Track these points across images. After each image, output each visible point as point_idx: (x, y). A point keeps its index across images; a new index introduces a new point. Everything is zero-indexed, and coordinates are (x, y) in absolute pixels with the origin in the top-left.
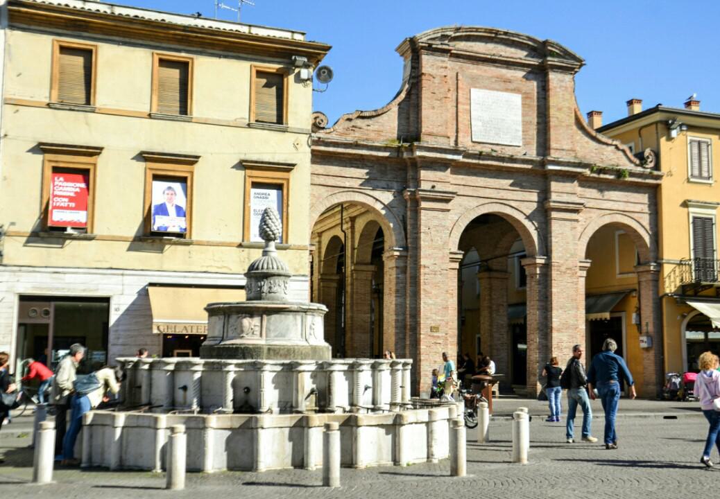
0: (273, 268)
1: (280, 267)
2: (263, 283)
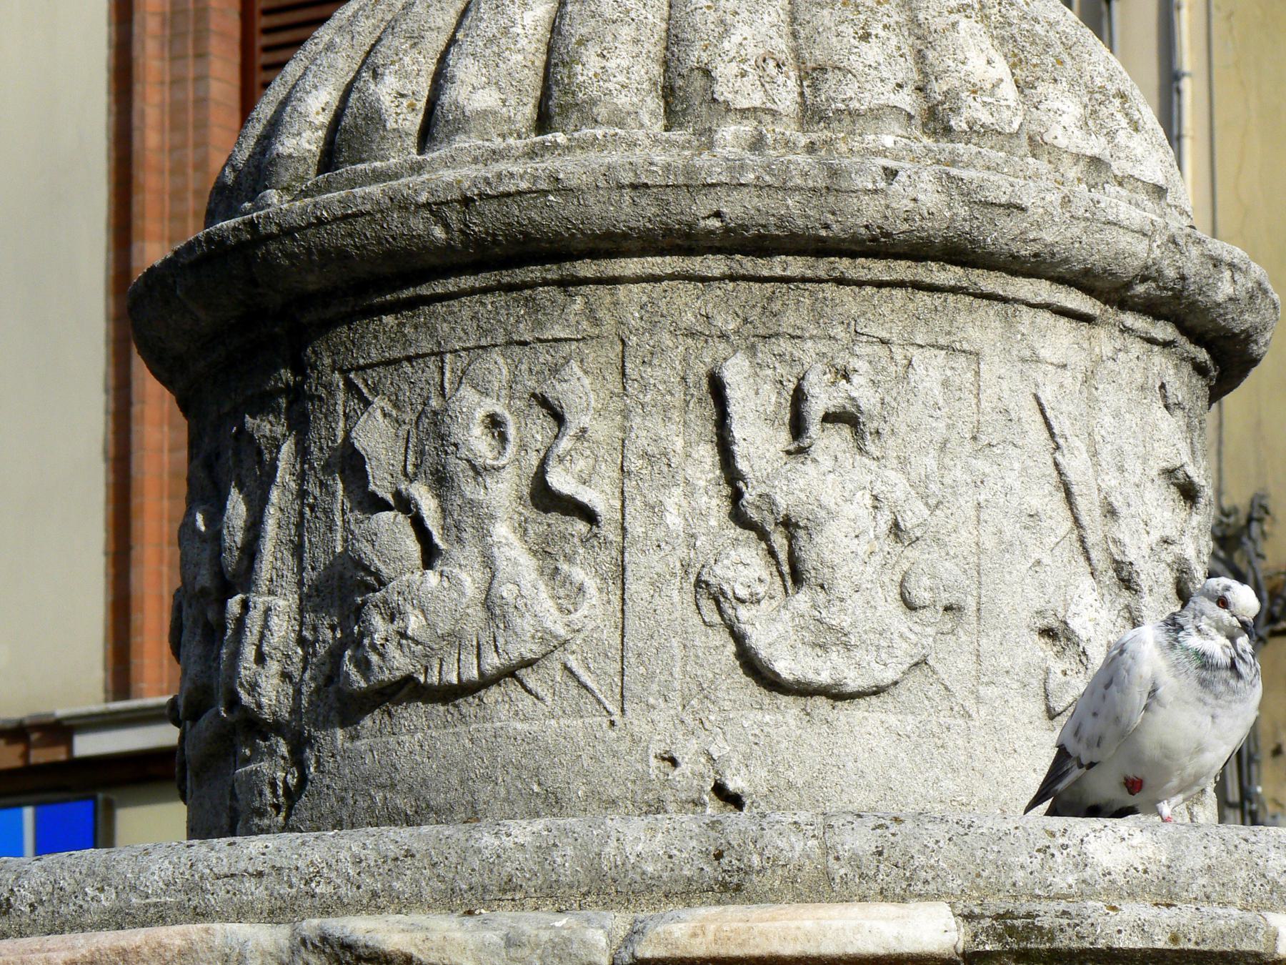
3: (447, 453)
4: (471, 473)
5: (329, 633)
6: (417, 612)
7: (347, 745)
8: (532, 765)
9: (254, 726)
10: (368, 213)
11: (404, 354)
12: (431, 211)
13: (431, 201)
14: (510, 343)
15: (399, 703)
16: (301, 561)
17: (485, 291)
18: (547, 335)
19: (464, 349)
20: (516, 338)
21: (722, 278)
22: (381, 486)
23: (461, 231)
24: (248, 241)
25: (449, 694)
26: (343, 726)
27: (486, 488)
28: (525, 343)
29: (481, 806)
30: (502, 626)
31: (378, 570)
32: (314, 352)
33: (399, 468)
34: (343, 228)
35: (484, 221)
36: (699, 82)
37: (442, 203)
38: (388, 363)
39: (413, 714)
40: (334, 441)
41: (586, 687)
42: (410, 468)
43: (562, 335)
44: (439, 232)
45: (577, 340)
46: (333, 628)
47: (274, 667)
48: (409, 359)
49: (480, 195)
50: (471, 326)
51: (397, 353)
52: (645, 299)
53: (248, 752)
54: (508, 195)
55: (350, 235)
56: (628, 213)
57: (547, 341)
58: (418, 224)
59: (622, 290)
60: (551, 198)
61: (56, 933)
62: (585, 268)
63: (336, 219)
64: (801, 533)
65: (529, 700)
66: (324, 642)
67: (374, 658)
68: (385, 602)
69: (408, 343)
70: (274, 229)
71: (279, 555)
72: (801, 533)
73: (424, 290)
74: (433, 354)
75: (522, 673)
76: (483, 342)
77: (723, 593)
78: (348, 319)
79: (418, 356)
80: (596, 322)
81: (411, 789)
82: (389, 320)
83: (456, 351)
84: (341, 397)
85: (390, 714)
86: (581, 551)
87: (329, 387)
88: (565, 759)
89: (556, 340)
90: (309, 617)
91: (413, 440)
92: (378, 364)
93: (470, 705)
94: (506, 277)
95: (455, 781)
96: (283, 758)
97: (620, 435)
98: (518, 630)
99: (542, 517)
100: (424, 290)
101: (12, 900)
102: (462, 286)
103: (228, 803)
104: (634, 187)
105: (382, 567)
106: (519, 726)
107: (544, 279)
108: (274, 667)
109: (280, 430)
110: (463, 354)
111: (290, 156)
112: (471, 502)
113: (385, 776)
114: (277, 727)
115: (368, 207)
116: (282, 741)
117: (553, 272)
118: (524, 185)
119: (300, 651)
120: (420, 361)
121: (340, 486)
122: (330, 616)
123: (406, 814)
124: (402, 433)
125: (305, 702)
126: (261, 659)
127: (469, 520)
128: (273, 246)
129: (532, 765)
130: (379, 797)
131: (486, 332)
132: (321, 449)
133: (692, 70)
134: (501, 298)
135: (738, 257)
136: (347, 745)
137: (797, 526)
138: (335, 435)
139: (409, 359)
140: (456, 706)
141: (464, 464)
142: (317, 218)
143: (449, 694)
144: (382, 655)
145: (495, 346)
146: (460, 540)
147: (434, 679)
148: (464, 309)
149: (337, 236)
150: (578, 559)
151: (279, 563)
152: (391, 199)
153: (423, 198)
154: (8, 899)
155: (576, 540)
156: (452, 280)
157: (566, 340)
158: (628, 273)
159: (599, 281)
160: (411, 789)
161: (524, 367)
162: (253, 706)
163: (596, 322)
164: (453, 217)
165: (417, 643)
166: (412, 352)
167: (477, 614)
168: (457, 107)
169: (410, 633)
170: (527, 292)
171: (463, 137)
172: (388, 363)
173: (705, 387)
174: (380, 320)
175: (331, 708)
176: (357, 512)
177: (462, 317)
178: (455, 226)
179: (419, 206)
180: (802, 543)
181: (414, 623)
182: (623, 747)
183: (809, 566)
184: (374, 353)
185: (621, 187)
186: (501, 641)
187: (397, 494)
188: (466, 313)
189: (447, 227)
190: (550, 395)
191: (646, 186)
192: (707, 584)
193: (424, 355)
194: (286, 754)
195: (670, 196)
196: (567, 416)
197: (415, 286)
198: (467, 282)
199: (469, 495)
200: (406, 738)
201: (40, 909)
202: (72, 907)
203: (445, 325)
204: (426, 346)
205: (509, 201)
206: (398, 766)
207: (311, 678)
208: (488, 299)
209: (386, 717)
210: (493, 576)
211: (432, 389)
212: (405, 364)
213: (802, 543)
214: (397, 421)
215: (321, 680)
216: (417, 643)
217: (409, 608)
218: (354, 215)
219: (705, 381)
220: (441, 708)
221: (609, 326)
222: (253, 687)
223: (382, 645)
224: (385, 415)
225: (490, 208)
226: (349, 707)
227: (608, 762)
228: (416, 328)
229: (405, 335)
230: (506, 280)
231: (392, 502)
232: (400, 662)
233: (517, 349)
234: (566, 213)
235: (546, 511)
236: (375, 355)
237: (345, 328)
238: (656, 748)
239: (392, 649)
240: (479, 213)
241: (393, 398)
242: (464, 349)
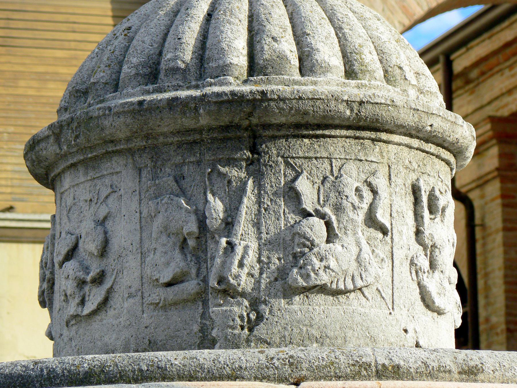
0: (307, 64)
1: (370, 57)
2: (217, 207)
3: (342, 199)
4: (352, 208)
5: (277, 261)
6: (334, 259)
7: (286, 306)
8: (366, 325)
9: (228, 292)
10: (323, 99)
11: (315, 156)
12: (347, 103)
13: (349, 100)
14: (355, 159)
15: (313, 293)
16: (259, 229)
17: (347, 137)
18: (369, 159)
19: (340, 158)
20: (359, 158)
21: (417, 149)
22: (309, 205)
23: (356, 114)
24: (259, 99)
25: (336, 293)
26: (284, 298)
27: (358, 215)
28: (361, 160)
29: (348, 339)
30: (363, 270)
31: (313, 240)
32: (266, 146)
33: (316, 200)
34: (311, 103)
35: (367, 111)
36: (398, 71)
37: (353, 101)
38: (306, 158)
39: (320, 299)
40: (280, 184)
41: (383, 298)
42: (322, 202)
43: (374, 160)
44: (348, 112)
45: (377, 163)
46: (279, 259)
47: (246, 270)
48: (316, 158)
49: (367, 101)
50: (342, 150)
51: (311, 154)
52: (396, 152)
53: (222, 302)
54: (377, 103)
55: (313, 106)
56: (408, 118)
57: (369, 161)
58: (342, 107)
59: (390, 146)
60: (390, 107)
61: (505, 383)
62: (384, 136)
63: (308, 99)
64: (437, 250)
65: (365, 299)
66: (274, 263)
67: (312, 274)
68: (319, 253)
69: (316, 151)
70: (276, 97)
71: (246, 225)
72: (437, 250)
73: (327, 132)
74: (327, 158)
75: (364, 289)
76: (347, 157)
77: (420, 269)
78: (287, 137)
79: (321, 158)
80: (382, 156)
81: (319, 328)
82: (306, 141)
83: (337, 158)
84: (282, 167)
85: (307, 297)
86: (380, 245)
87: (276, 163)
88: (377, 325)
89: (372, 161)
90: (265, 253)
91: (322, 191)
92: (301, 158)
93: (343, 298)
94: (358, 133)
95: (338, 328)
96: (246, 307)
97: (390, 203)
98: (371, 273)
99: (368, 229)
100: (327, 132)
101: (484, 367)
102: (342, 134)
103: (199, 321)
104: (414, 109)
105: (315, 238)
106: (360, 308)
107: (370, 137)
108: (246, 270)
109: (243, 175)
110: (339, 160)
111: (237, 65)
112: (352, 219)
113: (307, 321)
114: (243, 295)
115: (324, 97)
116: (245, 300)
117: (373, 135)
118: (383, 101)
119: (258, 265)
120: (321, 159)
121: (283, 203)
122: (278, 254)
123: (317, 338)
124: (316, 186)
125: (263, 286)
126: (241, 265)
127: (351, 226)
128: (272, 104)
129: (366, 325)
130: (305, 329)
131: (348, 154)
132: (272, 186)
133: (394, 65)
134: (353, 141)
135: (422, 141)
136: (286, 306)
137: (436, 247)
138: (280, 182)
139: (316, 158)
140: (337, 298)
141: (350, 204)
142: (299, 97)
143: (336, 293)
144: (316, 274)
145: (350, 159)
146: (346, 233)
147: (334, 286)
148: (341, 142)
149: (308, 106)
150: (379, 247)
151: (246, 229)
152: (332, 96)
153: (346, 98)
154: (481, 367)
155: (378, 240)
156: (338, 131)
157: (375, 162)
158: (396, 141)
159: (385, 142)
160: (319, 328)
161: (361, 170)
162: (236, 284)
163: (382, 156)
164: (355, 106)
165: (333, 271)
166: (318, 155)
167: (354, 264)
168: (325, 62)
169: (331, 267)
170: (362, 141)
171: (331, 75)
172: (306, 158)
173: (410, 189)
174: (302, 140)
175: (278, 291)
176: (292, 214)
177: (338, 145)
178: (356, 111)
179: (343, 101)
180: (437, 254)
181: (333, 263)
182: (394, 323)
183: (440, 263)
184: (300, 153)
185: (411, 108)
186: (364, 276)
187: (316, 211)
188: (340, 144)
189: (352, 110)
190: (373, 183)
191: (418, 110)
192: (416, 265)
193: (324, 158)
194: (248, 306)
195: (423, 115)
196: (379, 192)
197: (323, 130)
198: (344, 132)
199: (351, 217)
200: (317, 307)
201: (496, 373)
202: (511, 374)
203: (332, 147)
204: (325, 155)
205: (376, 106)
206: (314, 318)
207: (267, 277)
208: (348, 140)
209: (305, 298)
210: (361, 250)
211: (327, 172)
212: (314, 159)
213: (437, 254)
214: (313, 182)
215: (272, 279)
216: (333, 271)
217: (331, 257)
218: (317, 99)
219: (410, 186)
220: (331, 298)
221: (385, 161)
222: (237, 277)
223: (317, 270)
224: (308, 178)
225: (369, 107)
226: (290, 292)
227: (390, 328)
228: (319, 146)
229: (315, 148)
230: (358, 135)
231: (314, 214)
232: (324, 278)
233: (358, 162)
234: (393, 115)
235: (369, 227)
236: (301, 154)
237: (284, 140)
238: (403, 326)
239: (321, 272)
240: (365, 108)
241: (309, 172)
242: (340, 158)
